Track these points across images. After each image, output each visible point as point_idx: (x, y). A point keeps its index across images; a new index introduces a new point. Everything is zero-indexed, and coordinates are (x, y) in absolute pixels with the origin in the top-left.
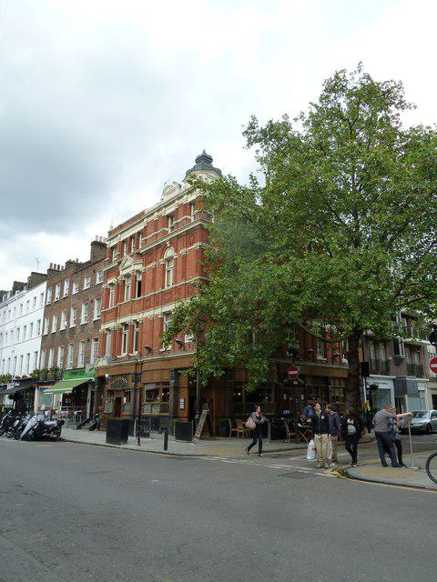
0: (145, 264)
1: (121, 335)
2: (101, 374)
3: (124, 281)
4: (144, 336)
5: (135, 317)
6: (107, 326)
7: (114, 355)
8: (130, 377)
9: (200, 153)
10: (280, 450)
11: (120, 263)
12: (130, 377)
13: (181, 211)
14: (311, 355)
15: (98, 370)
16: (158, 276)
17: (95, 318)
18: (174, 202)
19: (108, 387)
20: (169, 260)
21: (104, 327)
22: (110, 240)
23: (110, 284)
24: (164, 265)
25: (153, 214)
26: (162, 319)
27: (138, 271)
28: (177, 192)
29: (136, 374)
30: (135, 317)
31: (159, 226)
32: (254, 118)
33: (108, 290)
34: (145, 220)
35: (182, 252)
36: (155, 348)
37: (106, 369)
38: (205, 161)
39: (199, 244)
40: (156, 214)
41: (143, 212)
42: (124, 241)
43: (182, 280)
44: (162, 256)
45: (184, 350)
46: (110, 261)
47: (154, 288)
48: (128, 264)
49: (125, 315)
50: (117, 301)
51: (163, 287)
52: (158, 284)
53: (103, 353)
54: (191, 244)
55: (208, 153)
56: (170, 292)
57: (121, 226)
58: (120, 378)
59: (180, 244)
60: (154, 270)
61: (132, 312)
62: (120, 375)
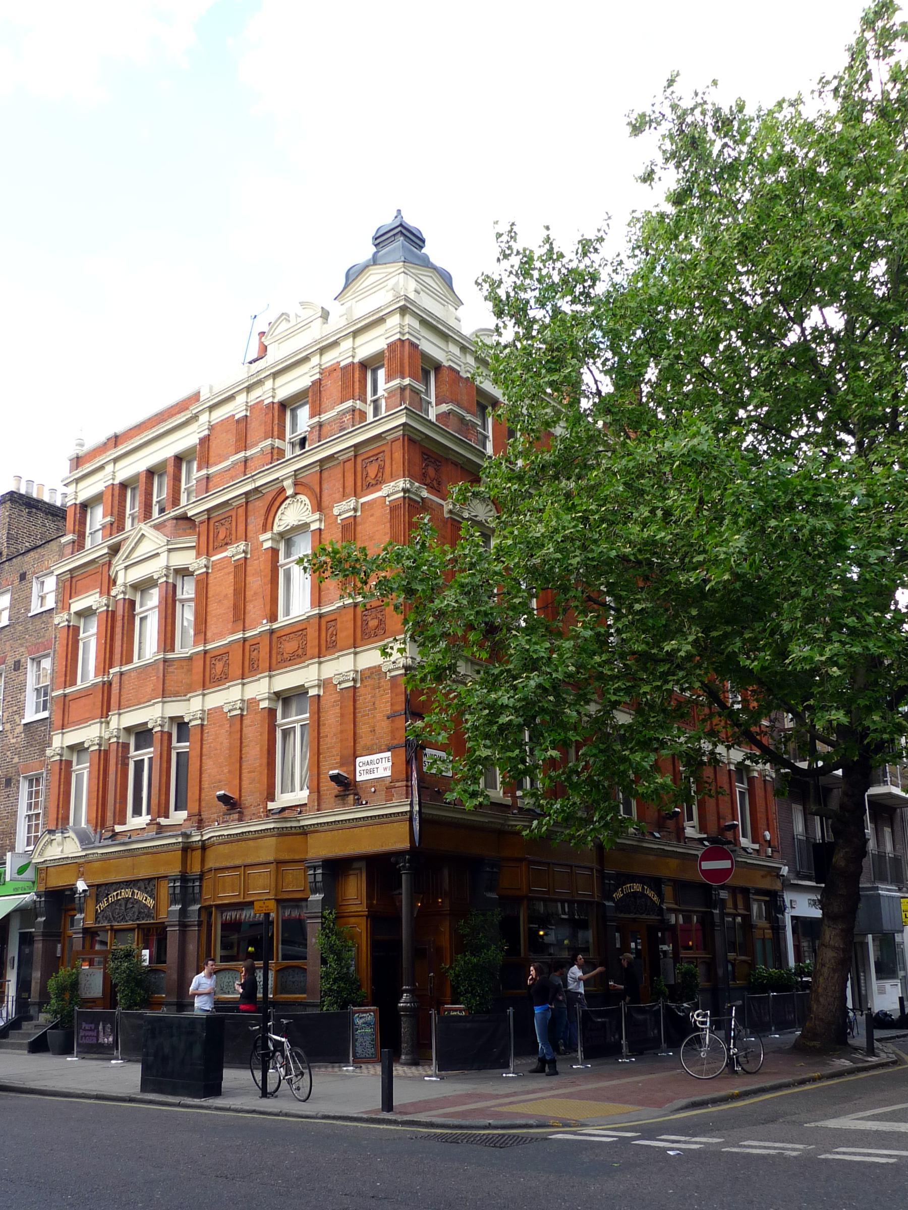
0: (207, 548)
1: (125, 765)
2: (57, 881)
3: (132, 603)
4: (209, 764)
5: (175, 709)
6: (73, 737)
7: (100, 821)
8: (164, 890)
9: (387, 220)
10: (511, 1103)
11: (115, 550)
12: (164, 890)
13: (332, 387)
14: (671, 823)
15: (42, 870)
16: (256, 583)
17: (31, 716)
18: (306, 359)
19: (83, 919)
20: (288, 537)
21: (59, 741)
22: (77, 481)
23: (79, 614)
24: (275, 552)
25: (231, 398)
26: (272, 712)
27: (183, 572)
28: (317, 332)
29: (184, 878)
30: (175, 709)
31: (252, 437)
32: (399, 211)
33: (73, 632)
34: (204, 418)
35: (343, 509)
36: (250, 799)
37: (78, 866)
38: (901, 9)
39: (401, 483)
40: (241, 399)
41: (196, 397)
42: (124, 486)
43: (196, 644)
44: (266, 526)
45: (358, 802)
46: (79, 544)
47: (240, 616)
48: (144, 549)
49: (139, 702)
50: (107, 660)
51: (273, 618)
52: (255, 608)
53: (61, 822)
54: (377, 483)
55: (411, 221)
56: (299, 630)
57: (116, 440)
58: (126, 893)
59: (332, 486)
60: (241, 568)
61: (165, 693)
62: (129, 884)
